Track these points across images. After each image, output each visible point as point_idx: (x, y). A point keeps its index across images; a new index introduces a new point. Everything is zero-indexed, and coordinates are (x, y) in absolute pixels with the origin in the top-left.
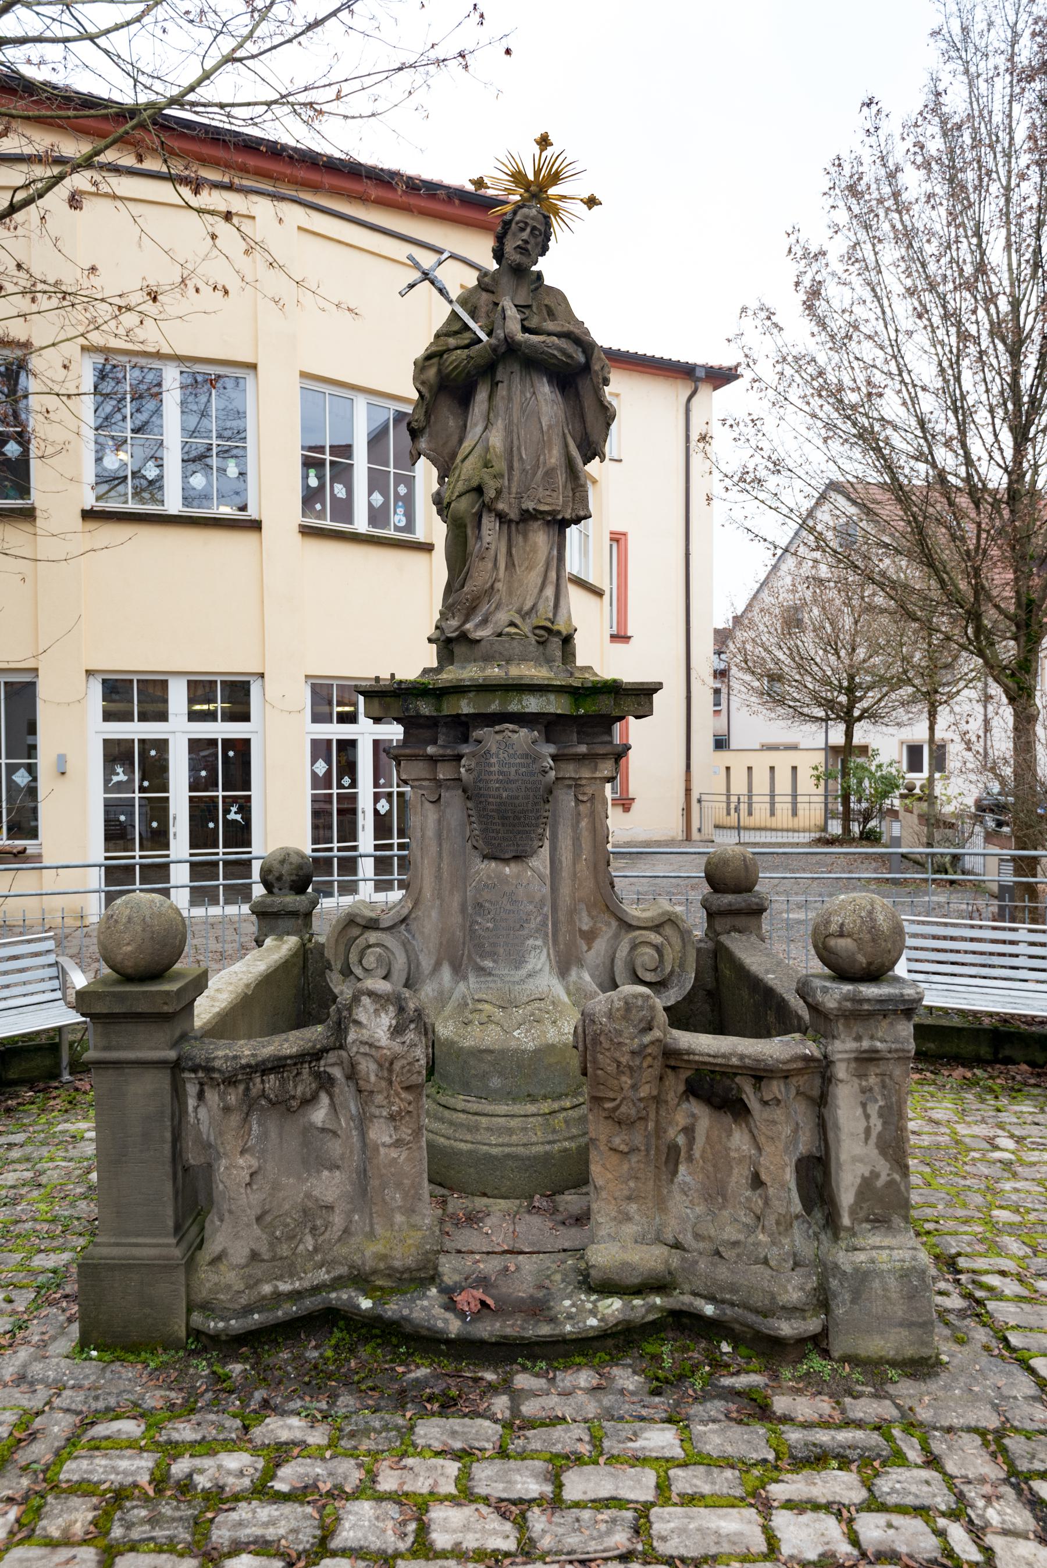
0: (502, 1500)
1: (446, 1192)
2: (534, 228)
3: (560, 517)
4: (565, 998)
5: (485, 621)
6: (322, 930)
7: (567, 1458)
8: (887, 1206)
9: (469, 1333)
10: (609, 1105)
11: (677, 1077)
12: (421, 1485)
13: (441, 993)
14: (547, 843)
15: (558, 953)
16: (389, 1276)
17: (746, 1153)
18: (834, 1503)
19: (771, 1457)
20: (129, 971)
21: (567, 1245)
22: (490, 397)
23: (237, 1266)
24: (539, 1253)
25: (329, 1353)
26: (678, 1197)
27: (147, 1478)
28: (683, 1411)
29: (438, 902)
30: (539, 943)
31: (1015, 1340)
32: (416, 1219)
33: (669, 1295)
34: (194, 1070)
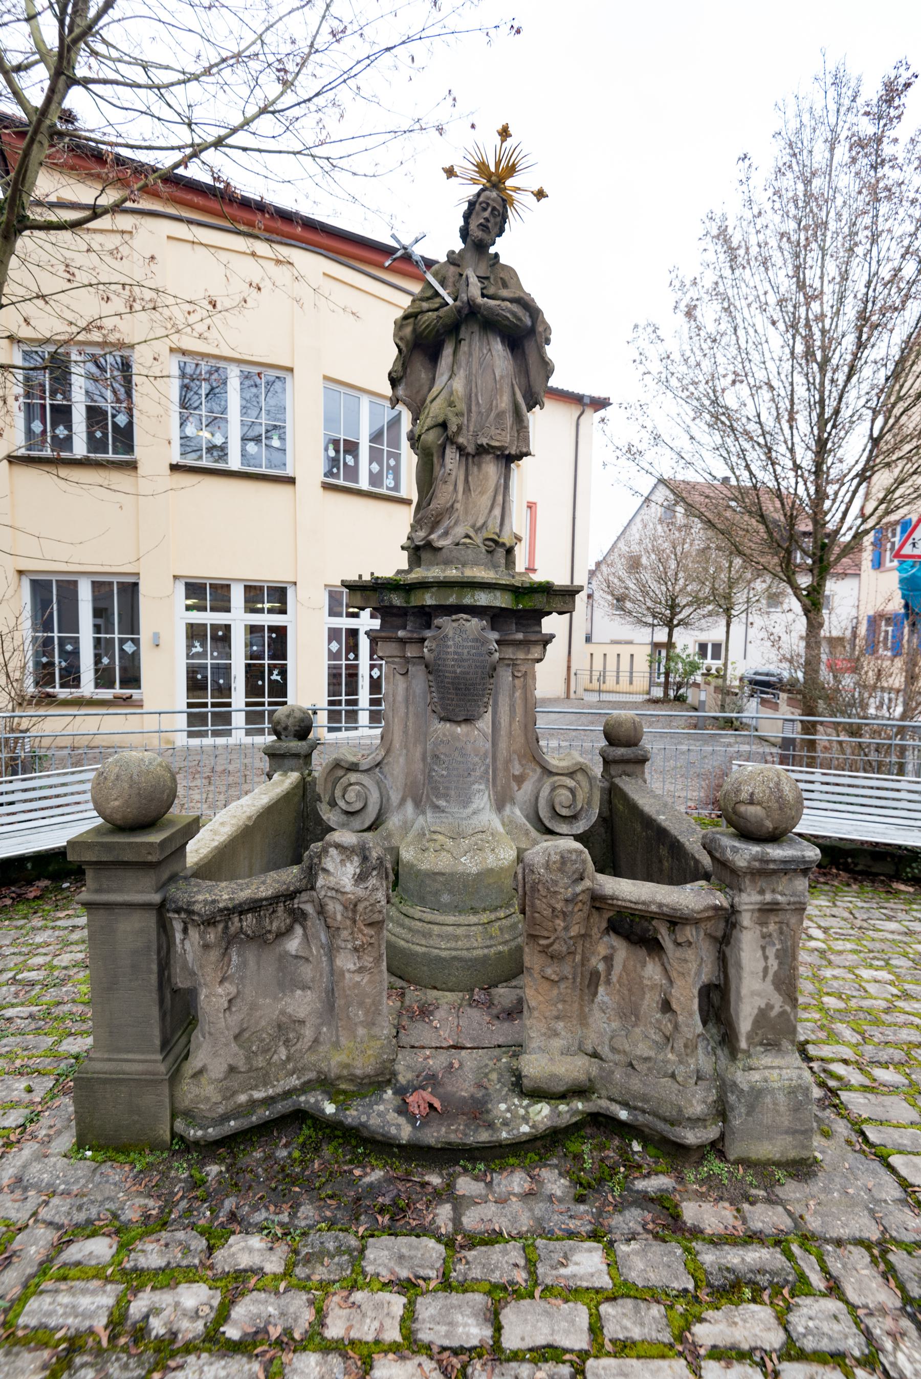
0: (444, 1349)
1: (404, 984)
2: (494, 209)
3: (507, 452)
4: (501, 829)
5: (446, 534)
6: (320, 763)
7: (504, 1289)
8: (777, 1032)
9: (418, 1139)
10: (543, 942)
11: (601, 916)
12: (366, 1332)
13: (405, 823)
14: (490, 708)
15: (496, 793)
16: (352, 1080)
17: (658, 982)
18: (756, 1349)
19: (691, 1286)
20: (119, 822)
21: (501, 1041)
22: (455, 353)
23: (216, 1080)
24: (478, 1048)
25: (296, 1154)
26: (597, 1014)
27: (104, 1321)
28: (606, 1223)
29: (404, 751)
30: (482, 787)
31: (872, 1136)
32: (376, 1031)
33: (589, 1100)
34: (178, 911)
